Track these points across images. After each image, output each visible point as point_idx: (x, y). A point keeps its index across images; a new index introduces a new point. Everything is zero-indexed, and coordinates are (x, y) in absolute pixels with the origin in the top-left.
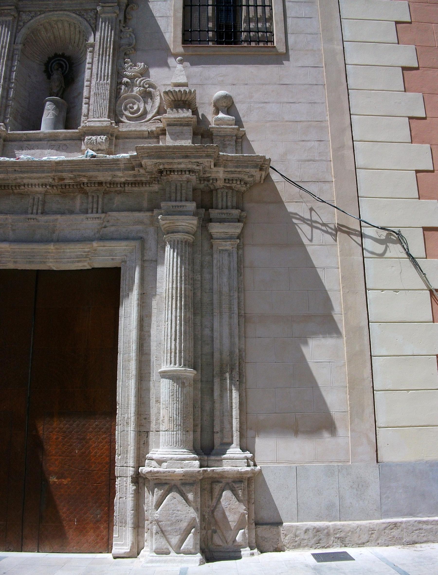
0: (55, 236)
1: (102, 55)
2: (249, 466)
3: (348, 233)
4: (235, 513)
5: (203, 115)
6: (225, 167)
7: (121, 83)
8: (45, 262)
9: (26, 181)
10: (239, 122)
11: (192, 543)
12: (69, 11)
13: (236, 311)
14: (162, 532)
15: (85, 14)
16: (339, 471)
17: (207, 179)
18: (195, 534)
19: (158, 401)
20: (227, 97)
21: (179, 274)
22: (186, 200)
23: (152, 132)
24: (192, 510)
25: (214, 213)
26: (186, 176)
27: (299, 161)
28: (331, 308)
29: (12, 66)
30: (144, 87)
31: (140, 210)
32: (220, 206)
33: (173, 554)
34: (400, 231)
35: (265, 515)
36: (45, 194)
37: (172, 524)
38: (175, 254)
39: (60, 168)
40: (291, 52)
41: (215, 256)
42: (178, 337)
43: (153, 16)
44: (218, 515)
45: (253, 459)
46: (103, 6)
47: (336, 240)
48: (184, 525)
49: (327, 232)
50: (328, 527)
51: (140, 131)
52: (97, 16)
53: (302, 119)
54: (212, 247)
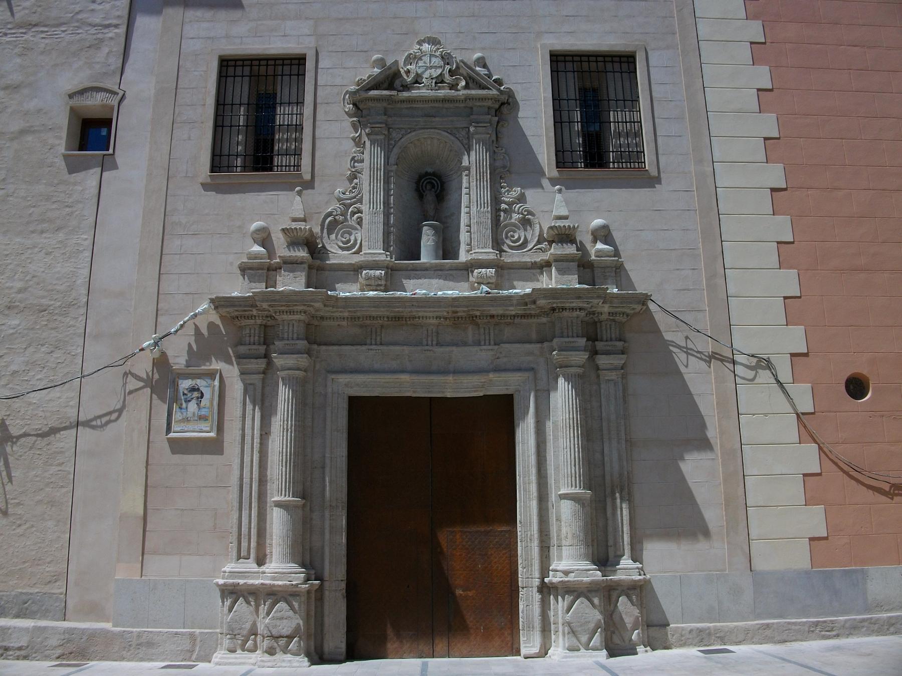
1: (480, 180)
3: (722, 361)
5: (581, 242)
6: (611, 303)
7: (500, 210)
8: (443, 392)
9: (420, 314)
10: (617, 253)
11: (599, 641)
12: (439, 129)
18: (601, 633)
19: (558, 520)
20: (605, 227)
23: (535, 262)
24: (598, 613)
25: (600, 345)
26: (575, 314)
28: (703, 426)
29: (389, 190)
31: (530, 342)
32: (605, 339)
33: (583, 650)
37: (581, 626)
40: (662, 175)
41: (602, 386)
43: (524, 135)
45: (642, 569)
48: (592, 626)
49: (701, 359)
50: (709, 628)
52: (469, 137)
54: (598, 376)
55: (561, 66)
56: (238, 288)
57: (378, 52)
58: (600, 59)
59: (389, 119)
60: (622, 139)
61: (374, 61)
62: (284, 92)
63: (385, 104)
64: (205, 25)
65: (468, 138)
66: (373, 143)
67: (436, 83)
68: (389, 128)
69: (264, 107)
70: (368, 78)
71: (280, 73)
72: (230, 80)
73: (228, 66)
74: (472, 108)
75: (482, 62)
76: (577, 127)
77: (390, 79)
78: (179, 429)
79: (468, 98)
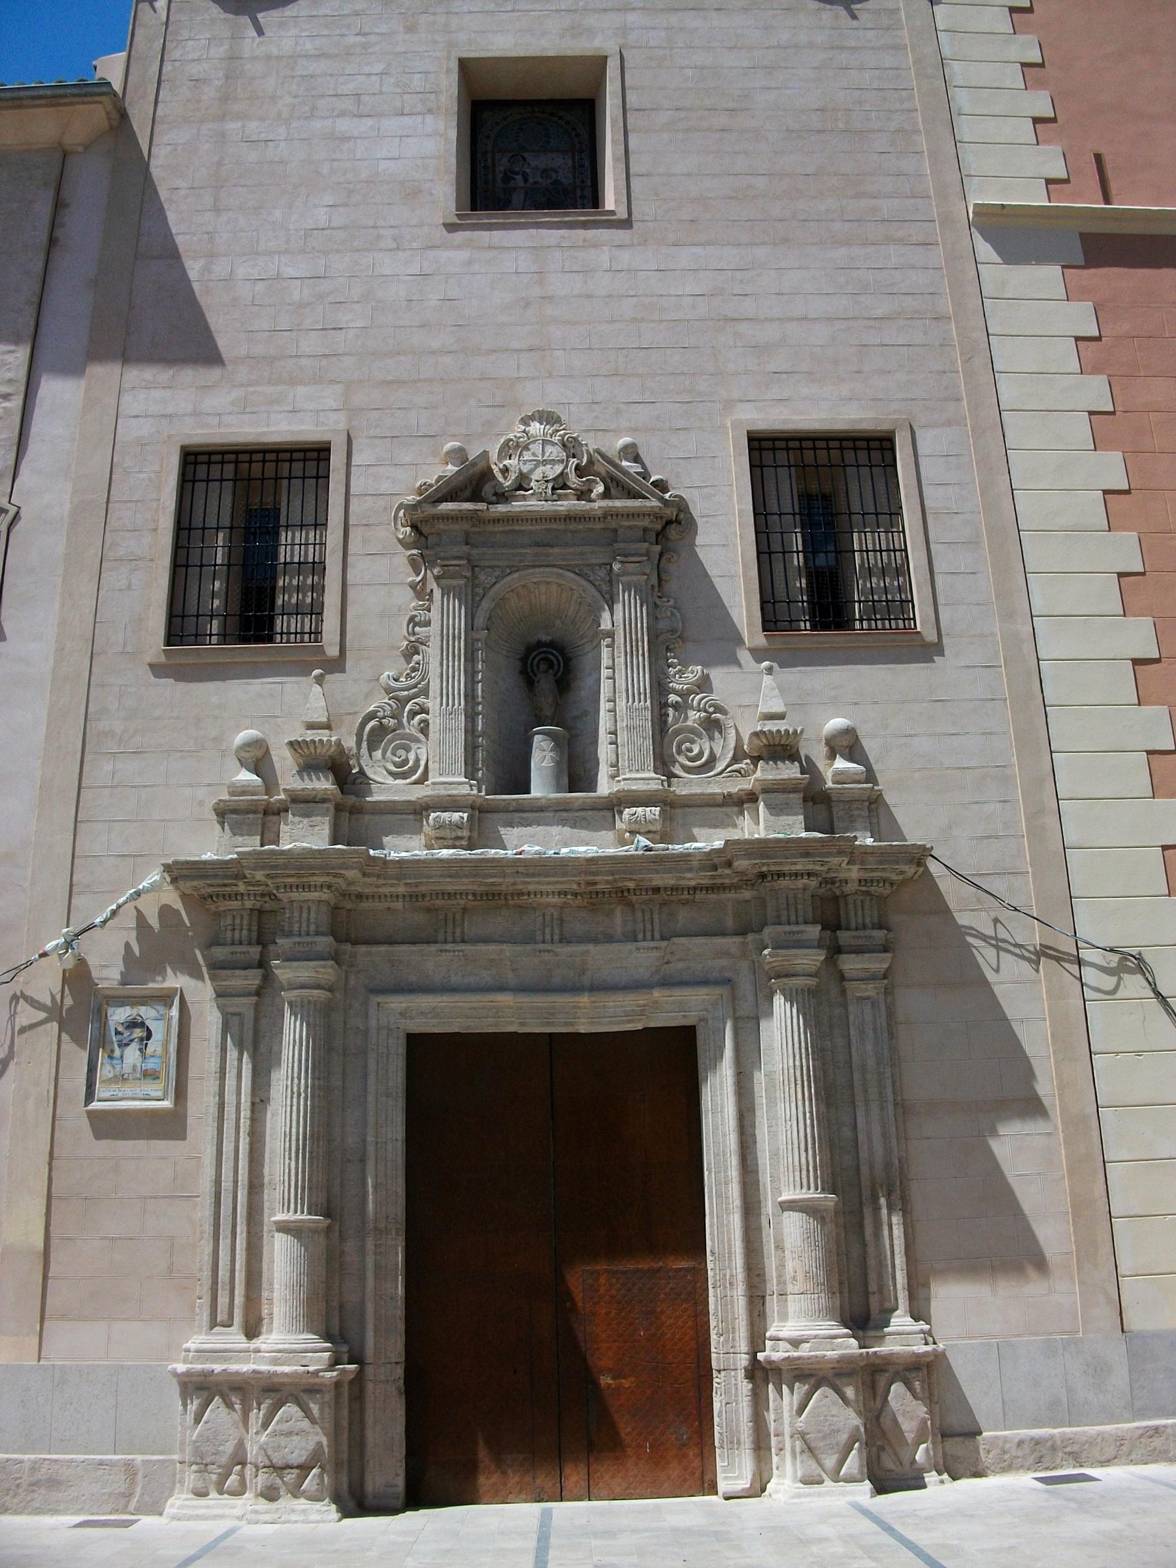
0: (586, 980)
1: (631, 653)
2: (926, 1344)
3: (1058, 960)
4: (912, 1419)
6: (862, 863)
7: (666, 705)
8: (572, 1024)
9: (531, 888)
10: (870, 777)
12: (560, 567)
13: (890, 1097)
14: (810, 1450)
15: (590, 573)
16: (1064, 1349)
17: (832, 881)
18: (860, 1450)
19: (779, 1247)
21: (803, 1044)
22: (806, 923)
23: (730, 795)
24: (853, 1415)
25: (844, 937)
27: (972, 838)
30: (706, 711)
31: (723, 934)
32: (853, 925)
33: (828, 1483)
34: (1140, 954)
35: (955, 1421)
36: (562, 907)
37: (824, 1438)
38: (794, 1010)
39: (593, 868)
40: (945, 641)
41: (851, 1008)
42: (810, 1146)
44: (886, 1421)
45: (929, 1333)
46: (622, 562)
47: (1037, 971)
48: (843, 1437)
49: (1023, 957)
50: (1052, 1437)
51: (710, 794)
53: (973, 763)
54: (843, 992)
55: (768, 457)
56: (213, 846)
57: (454, 437)
58: (832, 444)
59: (474, 552)
60: (874, 580)
61: (448, 453)
62: (292, 505)
63: (466, 526)
64: (157, 394)
65: (610, 581)
66: (445, 592)
67: (553, 489)
68: (474, 567)
69: (258, 533)
70: (437, 481)
71: (286, 474)
72: (201, 486)
73: (198, 464)
74: (615, 531)
75: (632, 453)
76: (797, 560)
77: (475, 483)
78: (107, 1095)
79: (608, 514)
